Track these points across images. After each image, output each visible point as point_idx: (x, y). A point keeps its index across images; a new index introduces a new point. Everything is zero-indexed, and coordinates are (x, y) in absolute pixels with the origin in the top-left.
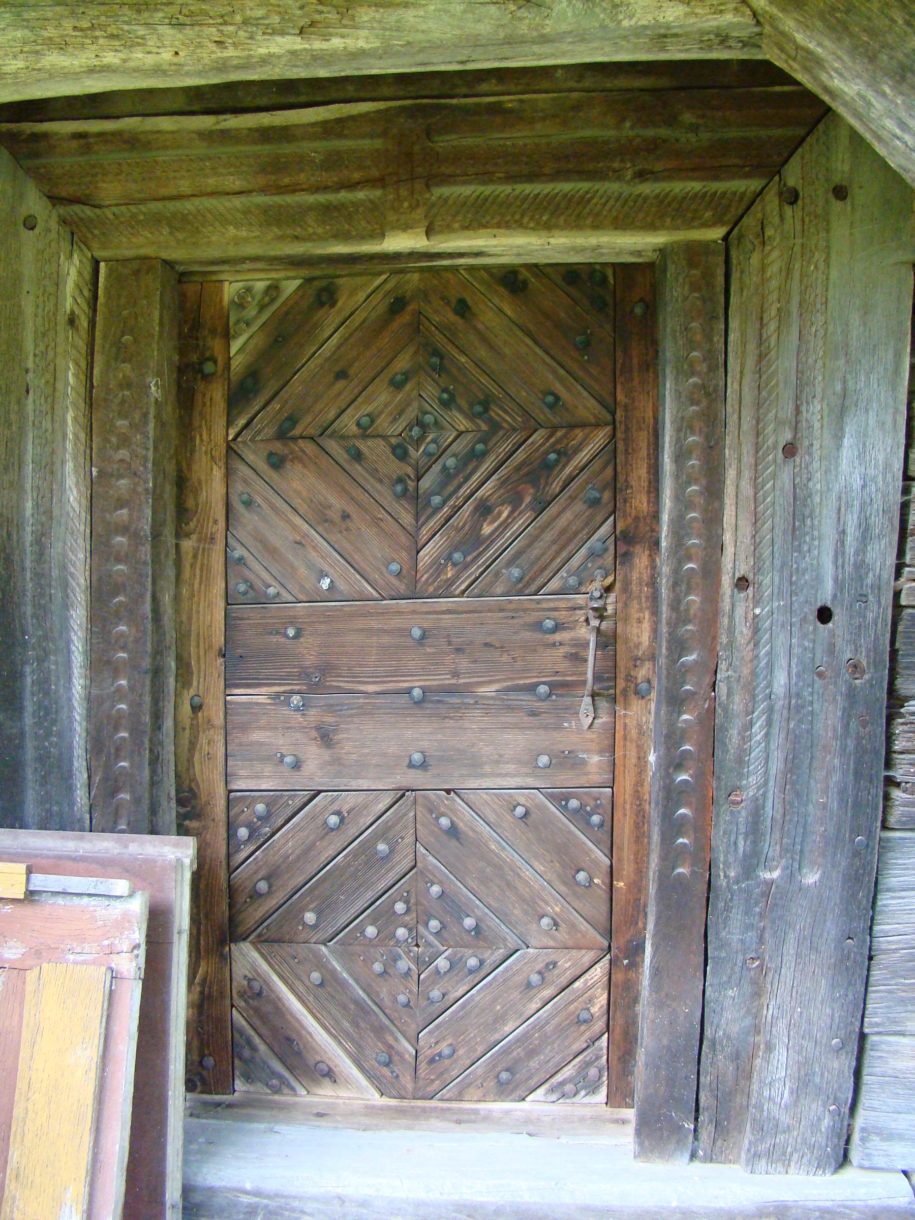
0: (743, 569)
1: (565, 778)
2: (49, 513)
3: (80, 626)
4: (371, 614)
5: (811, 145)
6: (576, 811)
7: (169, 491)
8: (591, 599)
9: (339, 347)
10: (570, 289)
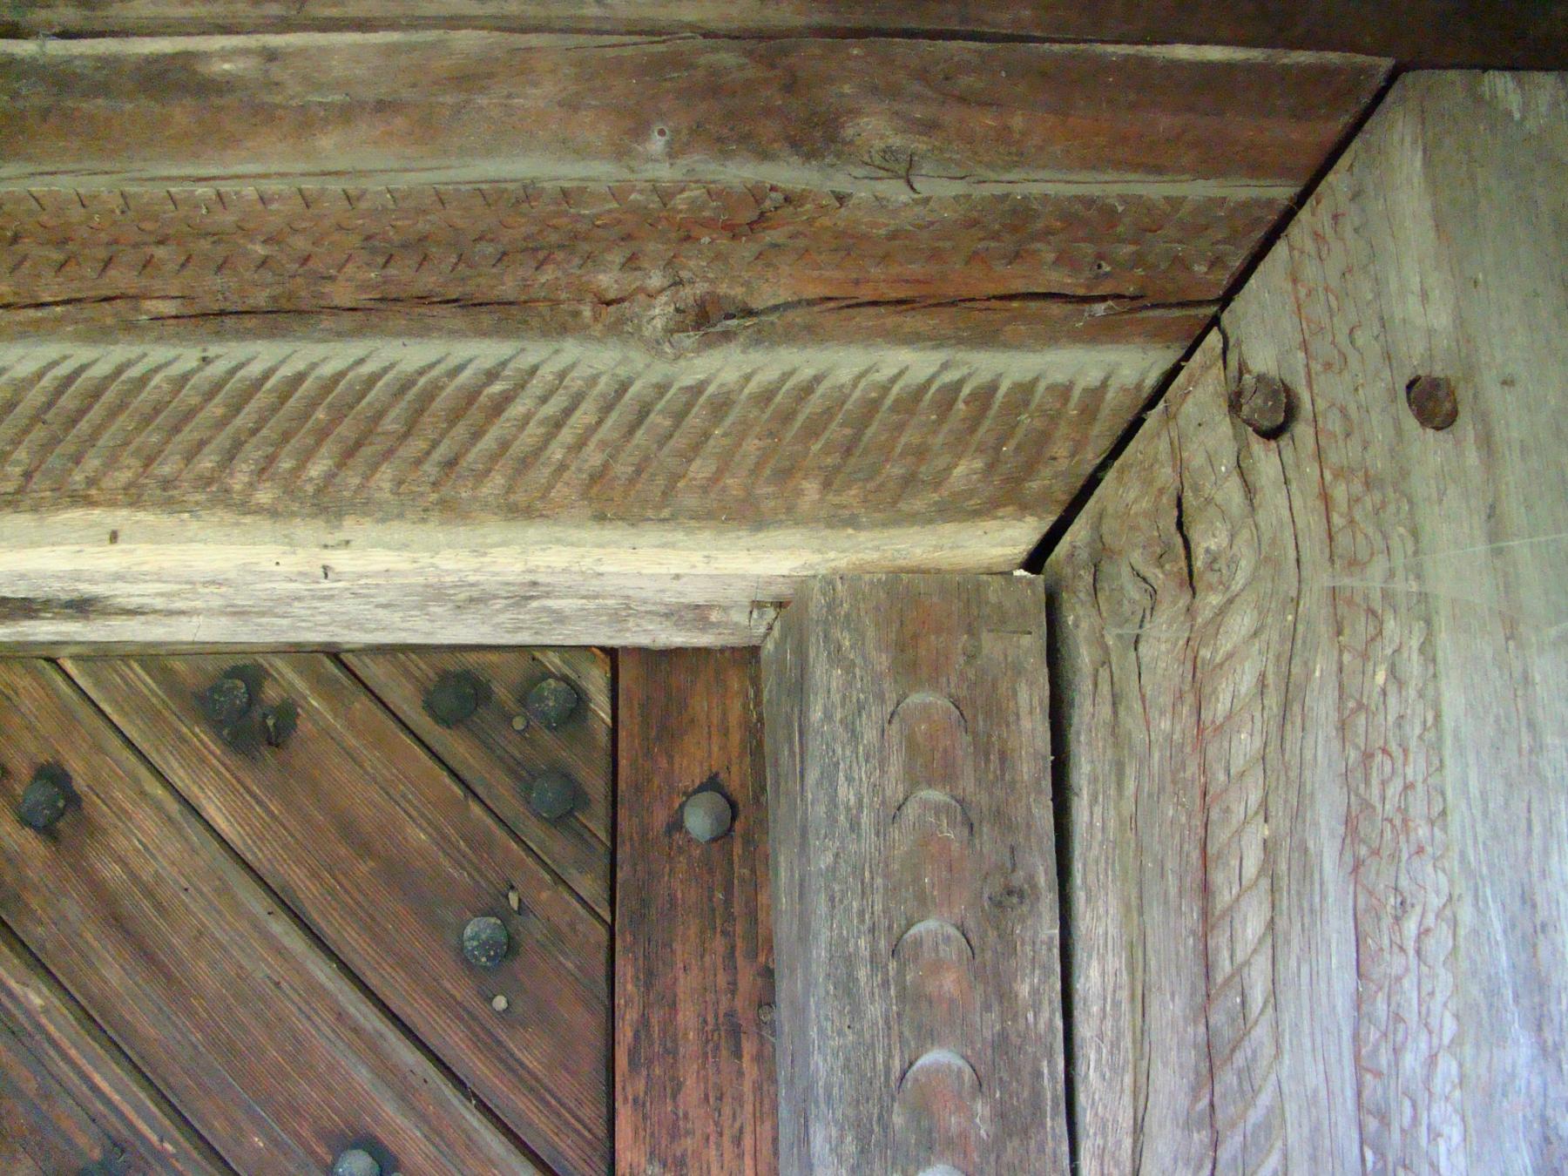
5: (1317, 236)
10: (457, 746)
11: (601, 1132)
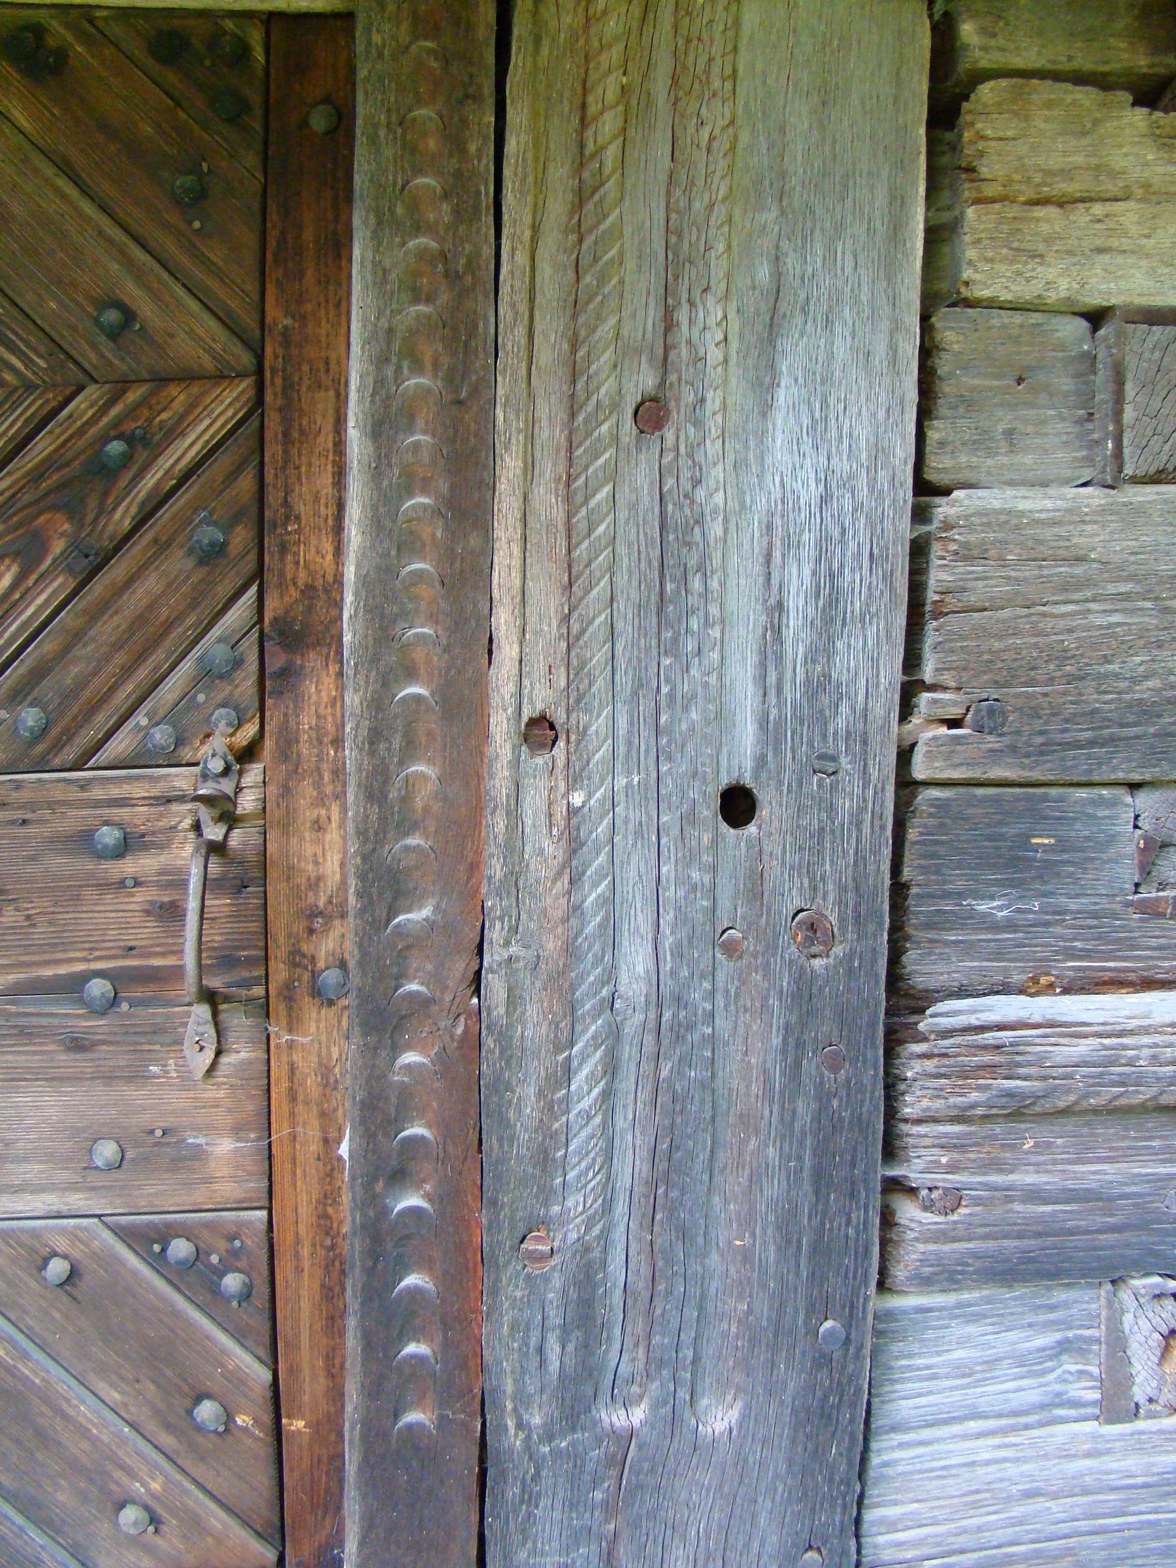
0: (540, 699)
1: (159, 1196)
6: (186, 1266)
8: (205, 776)
10: (171, 77)
11: (256, 298)
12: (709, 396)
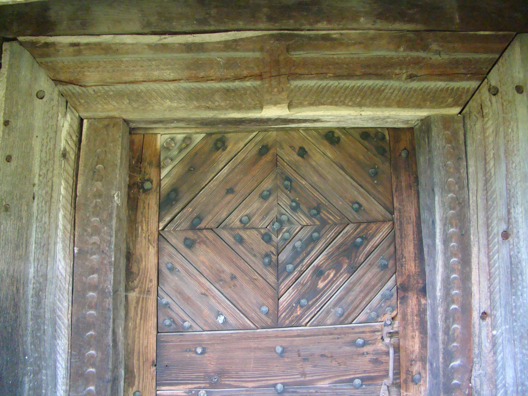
0: (484, 307)
2: (45, 276)
3: (64, 350)
4: (250, 338)
7: (123, 262)
9: (228, 175)
10: (366, 143)
12: (520, 231)
